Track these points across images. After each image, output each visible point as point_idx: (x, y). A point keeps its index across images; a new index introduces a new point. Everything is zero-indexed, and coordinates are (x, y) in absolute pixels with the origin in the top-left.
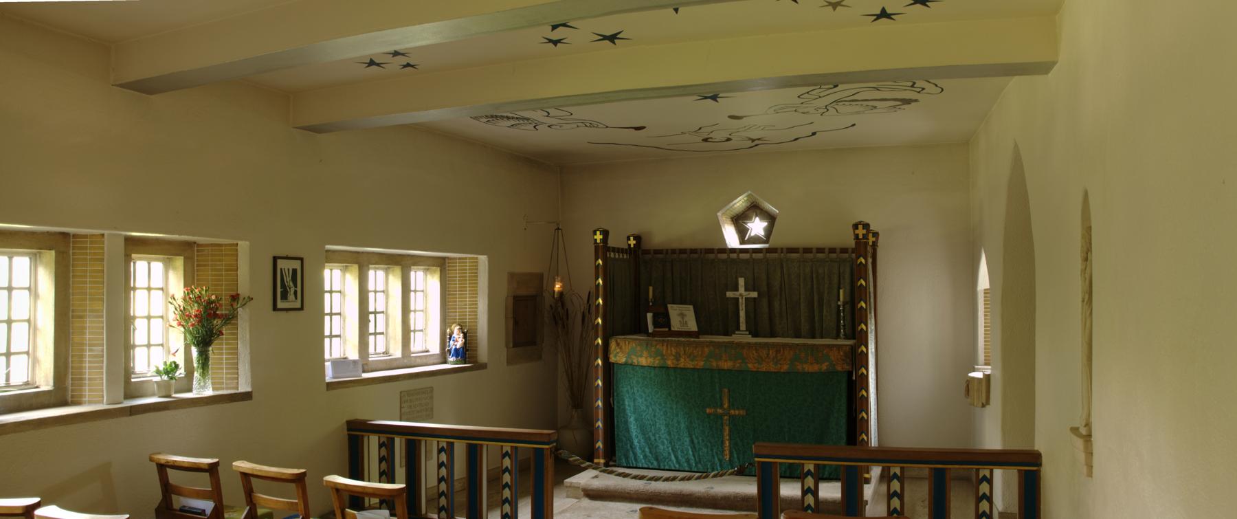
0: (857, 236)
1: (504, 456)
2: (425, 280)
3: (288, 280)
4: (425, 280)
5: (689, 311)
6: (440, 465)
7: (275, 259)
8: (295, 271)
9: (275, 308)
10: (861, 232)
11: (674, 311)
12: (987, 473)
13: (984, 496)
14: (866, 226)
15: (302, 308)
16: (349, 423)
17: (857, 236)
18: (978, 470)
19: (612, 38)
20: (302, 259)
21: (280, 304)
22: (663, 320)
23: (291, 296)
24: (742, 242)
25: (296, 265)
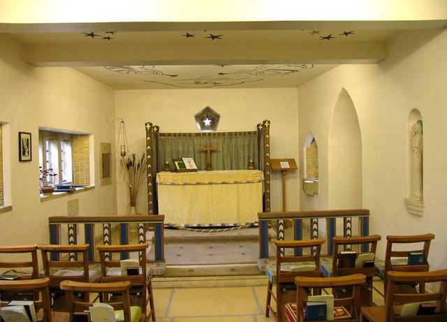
0: (147, 128)
1: (104, 229)
2: (49, 145)
3: (25, 144)
4: (49, 145)
5: (192, 160)
6: (70, 236)
7: (20, 133)
8: (28, 139)
9: (20, 160)
10: (148, 126)
11: (185, 160)
12: (316, 220)
13: (315, 229)
14: (151, 124)
15: (31, 160)
16: (50, 219)
17: (147, 128)
18: (278, 221)
19: (328, 38)
20: (30, 134)
21: (23, 158)
22: (182, 165)
23: (27, 154)
24: (202, 129)
25: (28, 136)
